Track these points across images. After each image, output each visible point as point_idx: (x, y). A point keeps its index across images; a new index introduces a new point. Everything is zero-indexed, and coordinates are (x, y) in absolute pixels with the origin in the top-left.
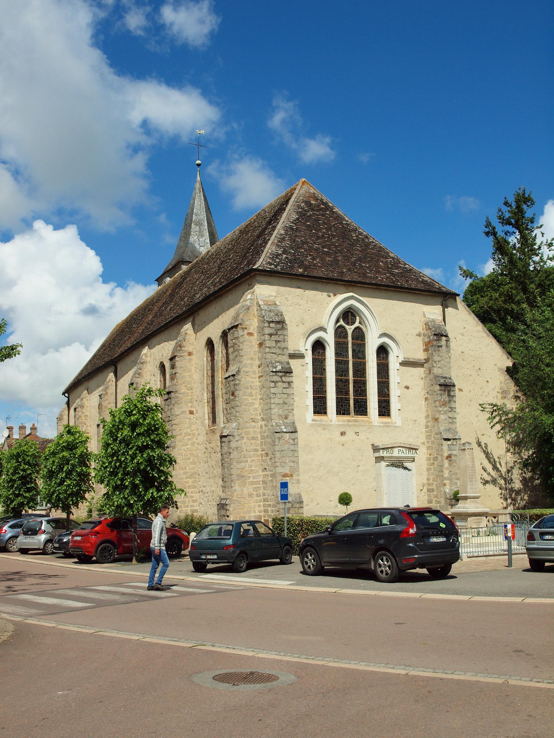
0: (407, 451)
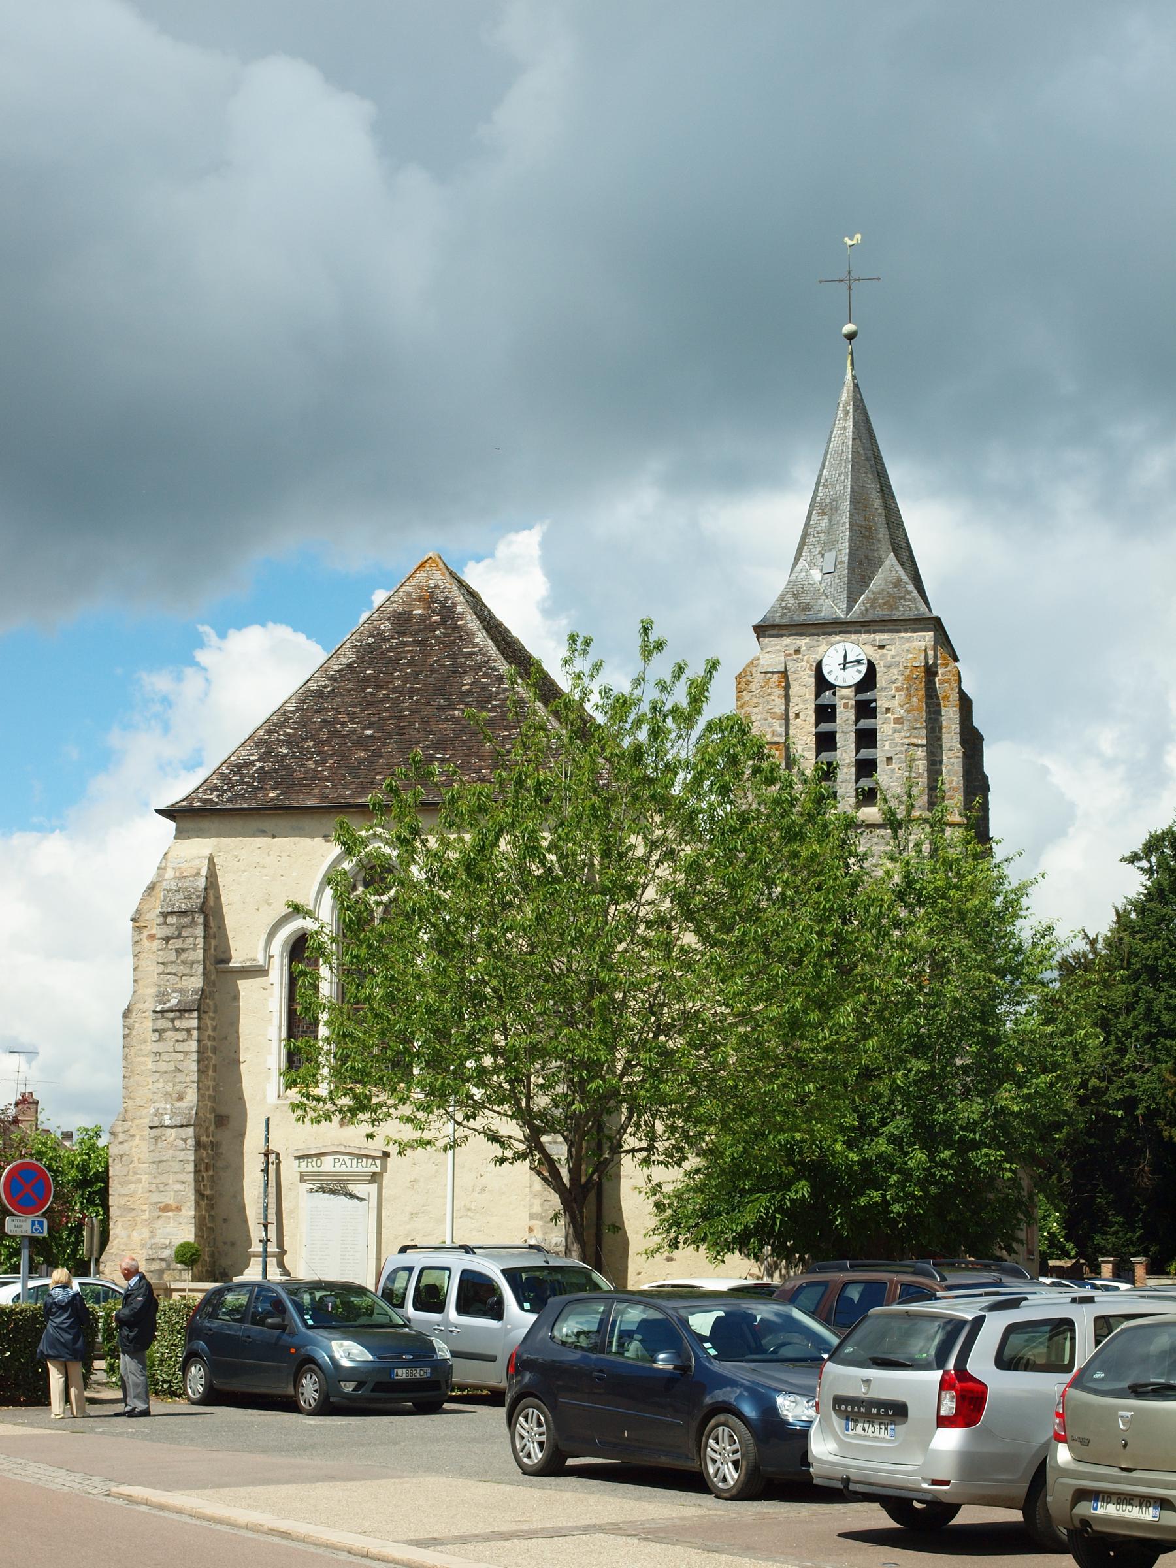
0: (355, 1161)
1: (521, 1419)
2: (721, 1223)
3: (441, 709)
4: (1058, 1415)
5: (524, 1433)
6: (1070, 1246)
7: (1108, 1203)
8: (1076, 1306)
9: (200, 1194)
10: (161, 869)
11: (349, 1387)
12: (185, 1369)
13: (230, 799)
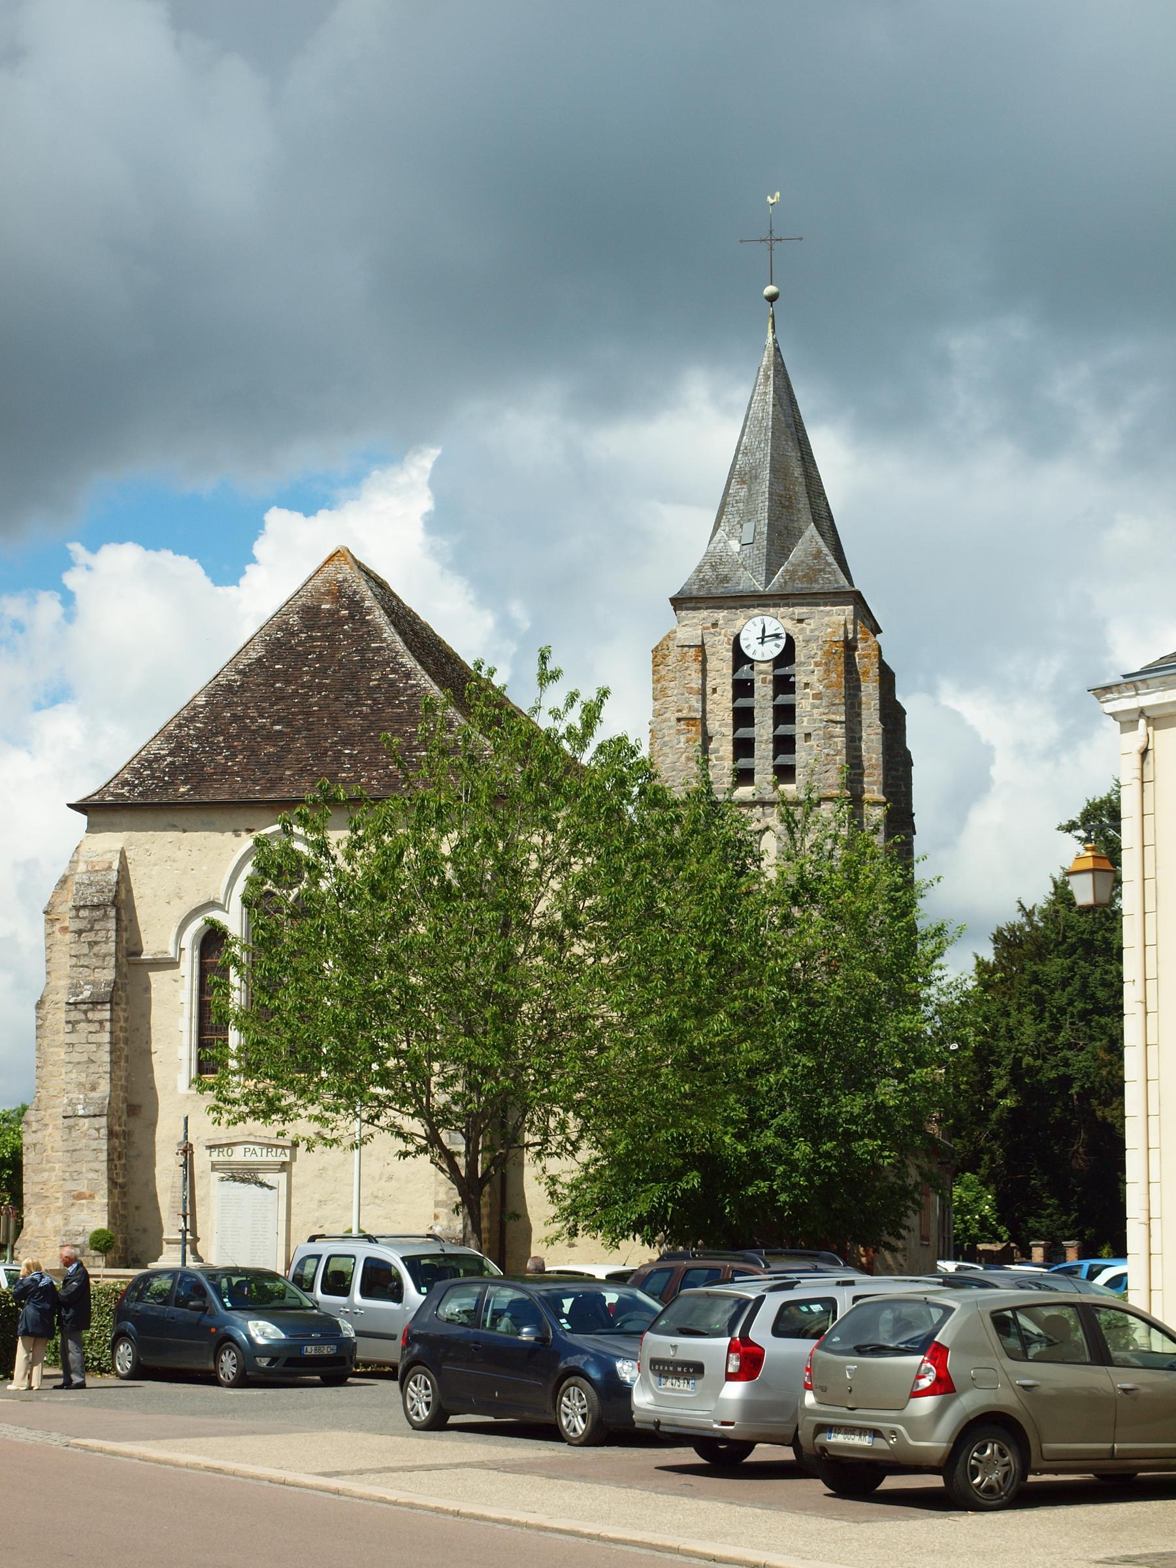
0: (265, 1151)
1: (411, 1383)
2: (616, 1212)
3: (349, 704)
4: (808, 1370)
5: (414, 1396)
6: (1002, 1229)
7: (1042, 1185)
8: (840, 1288)
9: (112, 1183)
10: (73, 863)
11: (264, 1362)
12: (114, 1347)
13: (141, 794)
